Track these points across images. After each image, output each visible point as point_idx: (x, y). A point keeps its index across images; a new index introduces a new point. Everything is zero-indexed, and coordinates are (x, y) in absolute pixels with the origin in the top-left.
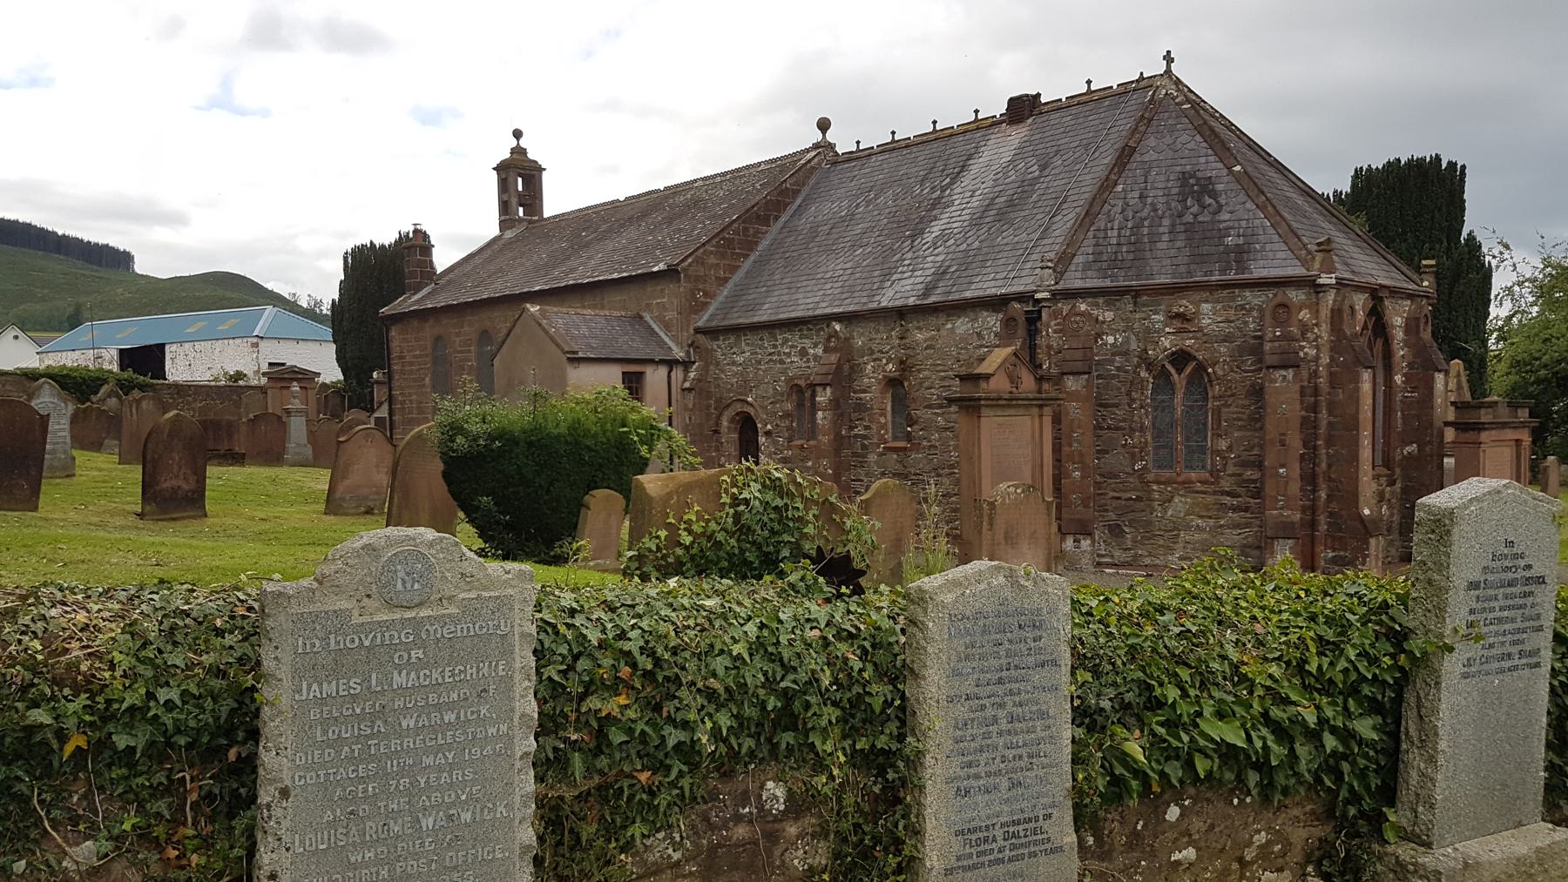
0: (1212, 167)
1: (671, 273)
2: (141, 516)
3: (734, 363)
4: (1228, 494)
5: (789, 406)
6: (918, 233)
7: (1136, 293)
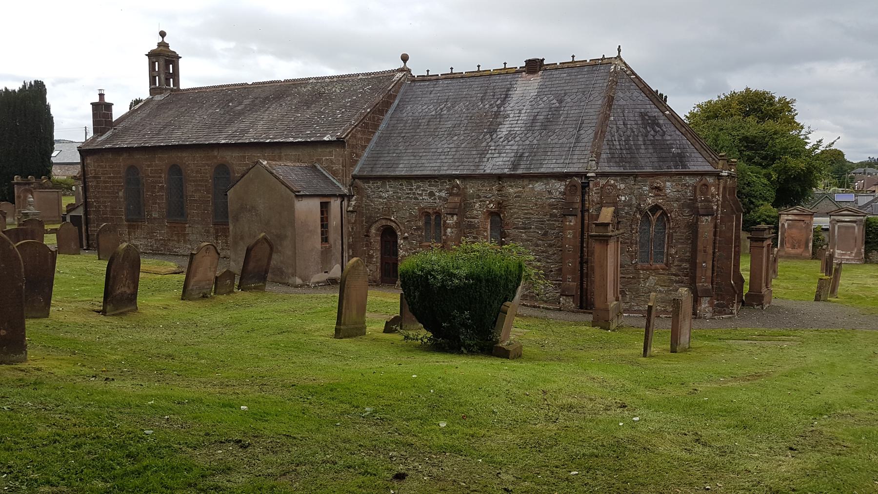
0: (655, 112)
1: (339, 143)
2: (104, 312)
3: (380, 197)
4: (674, 275)
5: (420, 224)
6: (492, 131)
7: (635, 176)
